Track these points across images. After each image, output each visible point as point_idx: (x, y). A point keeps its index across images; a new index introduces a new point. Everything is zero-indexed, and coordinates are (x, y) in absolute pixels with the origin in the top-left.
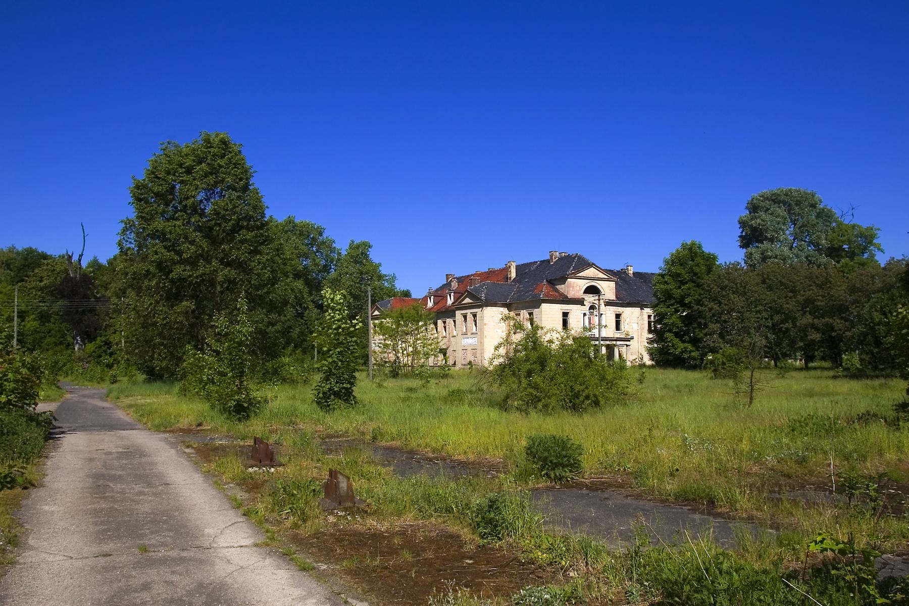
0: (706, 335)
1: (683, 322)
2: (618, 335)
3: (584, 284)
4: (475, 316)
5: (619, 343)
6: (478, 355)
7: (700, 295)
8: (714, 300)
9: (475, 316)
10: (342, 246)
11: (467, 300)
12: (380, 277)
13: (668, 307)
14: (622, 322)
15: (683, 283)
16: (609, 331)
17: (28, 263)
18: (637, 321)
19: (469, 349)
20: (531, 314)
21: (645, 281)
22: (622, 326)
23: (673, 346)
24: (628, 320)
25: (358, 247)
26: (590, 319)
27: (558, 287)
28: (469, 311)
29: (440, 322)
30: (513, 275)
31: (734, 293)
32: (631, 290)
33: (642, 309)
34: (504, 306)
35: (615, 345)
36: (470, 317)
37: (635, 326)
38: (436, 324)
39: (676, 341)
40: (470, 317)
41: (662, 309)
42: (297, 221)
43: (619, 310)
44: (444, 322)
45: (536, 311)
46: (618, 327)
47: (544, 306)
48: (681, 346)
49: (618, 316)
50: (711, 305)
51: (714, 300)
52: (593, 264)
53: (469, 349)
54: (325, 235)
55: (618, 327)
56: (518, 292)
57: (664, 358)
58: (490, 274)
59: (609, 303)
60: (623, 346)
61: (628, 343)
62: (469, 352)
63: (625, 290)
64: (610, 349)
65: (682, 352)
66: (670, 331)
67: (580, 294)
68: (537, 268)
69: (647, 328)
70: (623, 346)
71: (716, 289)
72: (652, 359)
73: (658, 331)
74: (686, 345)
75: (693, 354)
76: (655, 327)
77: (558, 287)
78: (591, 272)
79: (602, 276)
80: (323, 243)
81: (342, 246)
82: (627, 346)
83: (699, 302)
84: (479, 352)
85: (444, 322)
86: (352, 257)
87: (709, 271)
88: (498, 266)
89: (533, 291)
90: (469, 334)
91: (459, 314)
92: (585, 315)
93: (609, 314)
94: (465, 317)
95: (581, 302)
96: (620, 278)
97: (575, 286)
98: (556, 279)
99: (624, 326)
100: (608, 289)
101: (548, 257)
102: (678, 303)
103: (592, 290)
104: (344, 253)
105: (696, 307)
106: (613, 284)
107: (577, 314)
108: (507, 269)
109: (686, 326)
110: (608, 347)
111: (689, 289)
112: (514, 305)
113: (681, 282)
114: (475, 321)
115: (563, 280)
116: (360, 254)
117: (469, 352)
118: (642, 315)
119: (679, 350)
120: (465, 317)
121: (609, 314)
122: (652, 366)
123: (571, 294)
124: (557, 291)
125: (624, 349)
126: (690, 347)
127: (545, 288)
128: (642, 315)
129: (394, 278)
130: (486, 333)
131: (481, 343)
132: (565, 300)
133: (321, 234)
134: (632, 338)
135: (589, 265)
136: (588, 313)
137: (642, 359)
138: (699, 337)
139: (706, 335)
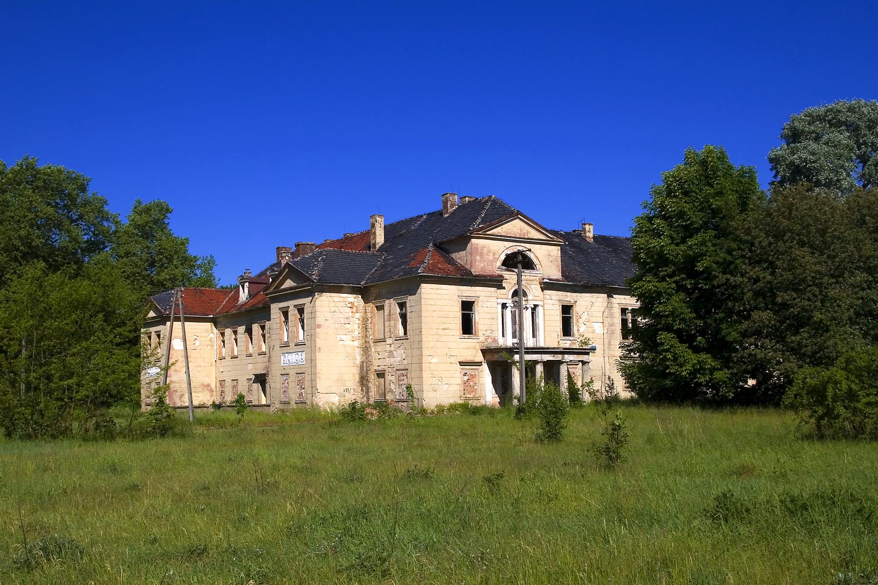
0: (745, 334)
1: (696, 310)
2: (567, 343)
3: (499, 250)
4: (301, 311)
5: (568, 358)
6: (307, 384)
7: (730, 252)
8: (759, 262)
9: (301, 311)
10: (122, 213)
11: (289, 283)
12: (186, 260)
13: (663, 279)
14: (574, 320)
15: (689, 231)
16: (549, 334)
17: (829, 419)
18: (601, 318)
19: (292, 373)
20: (402, 306)
21: (615, 251)
22: (575, 329)
23: (675, 359)
24: (585, 317)
25: (148, 211)
26: (513, 314)
27: (454, 255)
28: (291, 304)
29: (256, 328)
30: (380, 238)
31: (802, 244)
32: (585, 269)
33: (610, 296)
34: (354, 291)
35: (560, 362)
36: (293, 313)
37: (598, 329)
38: (249, 331)
39: (682, 349)
40: (293, 313)
41: (650, 284)
42: (42, 167)
43: (569, 297)
44: (263, 328)
45: (410, 300)
46: (567, 330)
47: (426, 289)
48: (693, 359)
49: (566, 309)
50: (756, 271)
51: (755, 262)
52: (519, 213)
53: (292, 373)
54: (89, 194)
55: (567, 330)
56: (383, 266)
57: (657, 382)
58: (347, 241)
59: (548, 285)
60: (575, 363)
61: (584, 358)
62: (292, 378)
63: (580, 264)
64: (552, 369)
65: (694, 373)
66: (668, 329)
67: (495, 267)
68: (421, 225)
69: (619, 326)
70: (575, 363)
71: (763, 240)
72: (632, 386)
73: (639, 335)
74: (703, 356)
75: (718, 375)
76: (634, 322)
77: (454, 255)
78: (515, 227)
79: (535, 234)
80: (86, 203)
81: (122, 213)
82: (584, 363)
83: (727, 267)
84: (308, 378)
85: (263, 328)
86: (137, 226)
87: (743, 205)
88: (355, 230)
89: (408, 263)
90: (292, 345)
91: (275, 309)
92: (504, 306)
93: (550, 305)
94: (285, 314)
95: (496, 282)
96: (572, 245)
97: (487, 252)
98: (450, 242)
99: (580, 328)
100: (548, 259)
101: (439, 207)
102: (680, 270)
103: (518, 261)
104: (126, 223)
105: (722, 278)
106: (555, 251)
107: (489, 304)
108: (369, 234)
109: (699, 317)
110: (547, 365)
111: (703, 243)
112: (374, 291)
113: (686, 228)
114: (302, 321)
115: (462, 241)
116: (150, 225)
117: (292, 378)
118: (609, 306)
119: (689, 367)
120: (285, 314)
121: (550, 305)
122: (631, 402)
123: (479, 267)
124: (452, 262)
125: (577, 370)
126: (709, 360)
127: (430, 257)
128: (609, 306)
129: (210, 263)
130: (319, 343)
131: (312, 361)
132: (466, 278)
133: (83, 189)
134: (593, 349)
135: (508, 215)
136: (510, 303)
137: (611, 387)
138: (730, 339)
139: (745, 334)
